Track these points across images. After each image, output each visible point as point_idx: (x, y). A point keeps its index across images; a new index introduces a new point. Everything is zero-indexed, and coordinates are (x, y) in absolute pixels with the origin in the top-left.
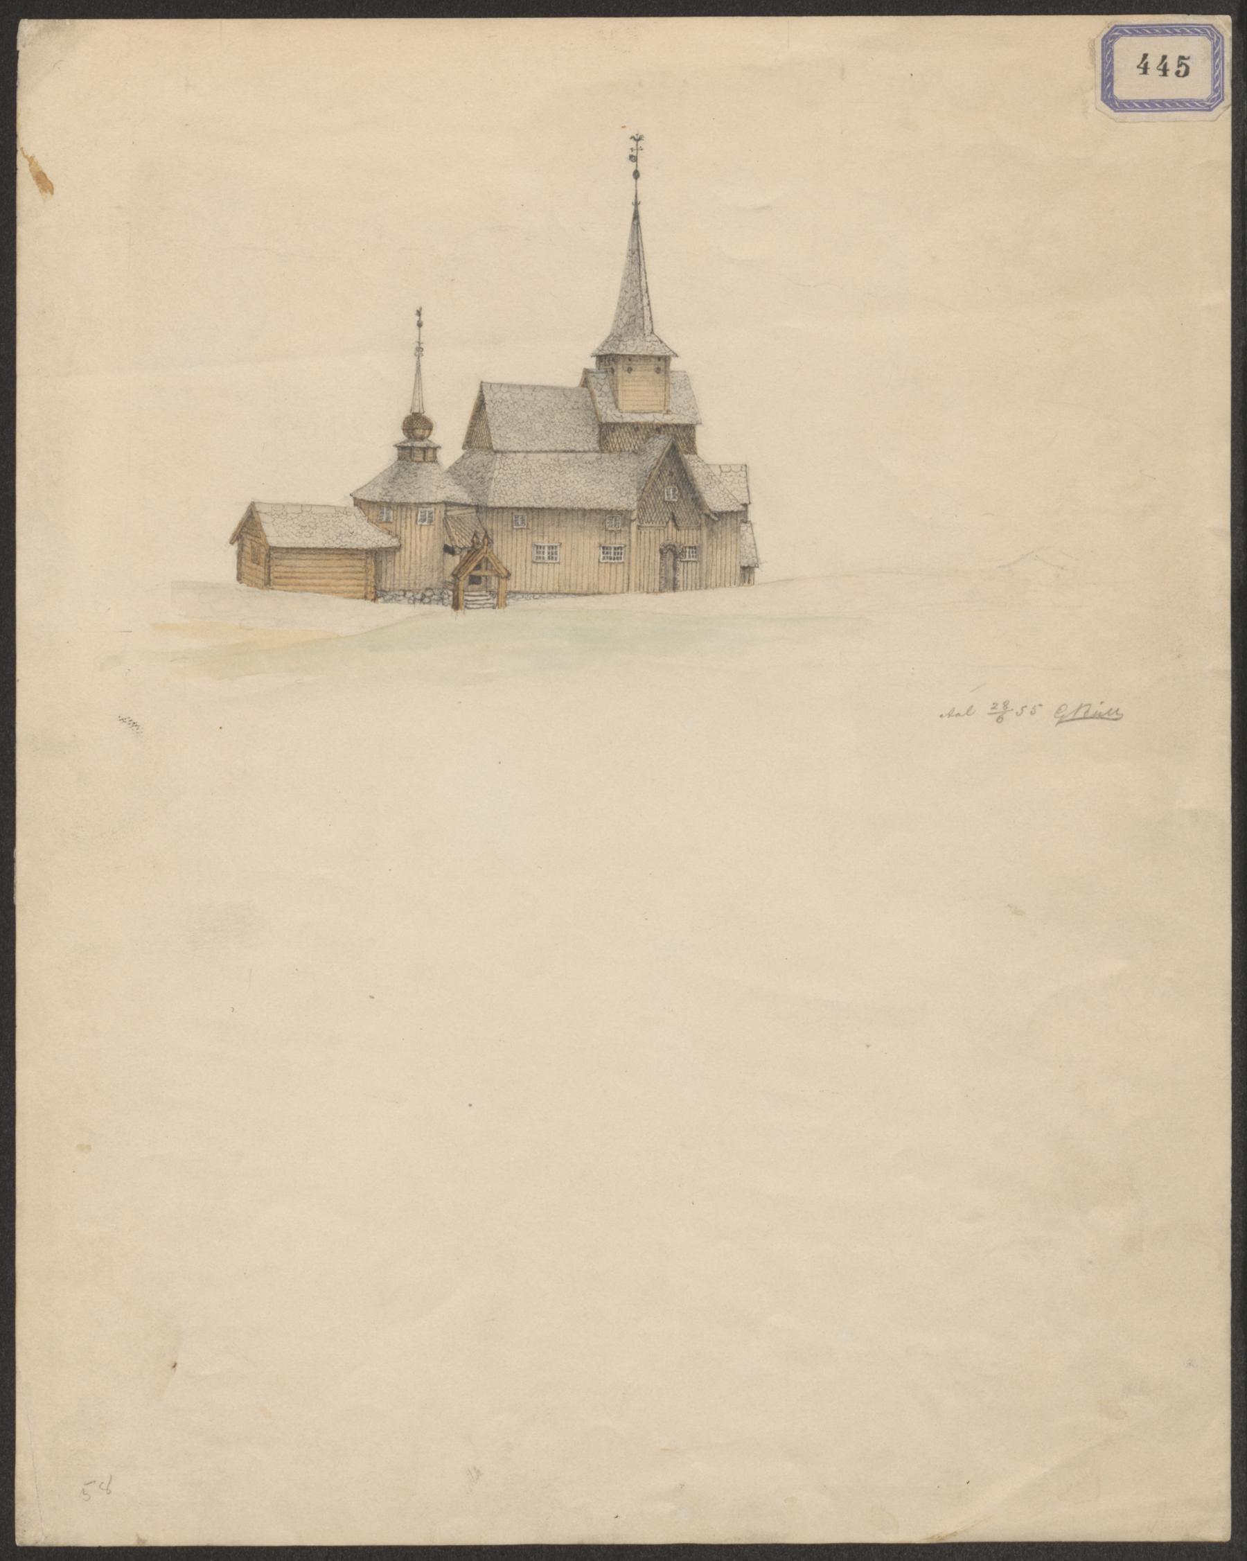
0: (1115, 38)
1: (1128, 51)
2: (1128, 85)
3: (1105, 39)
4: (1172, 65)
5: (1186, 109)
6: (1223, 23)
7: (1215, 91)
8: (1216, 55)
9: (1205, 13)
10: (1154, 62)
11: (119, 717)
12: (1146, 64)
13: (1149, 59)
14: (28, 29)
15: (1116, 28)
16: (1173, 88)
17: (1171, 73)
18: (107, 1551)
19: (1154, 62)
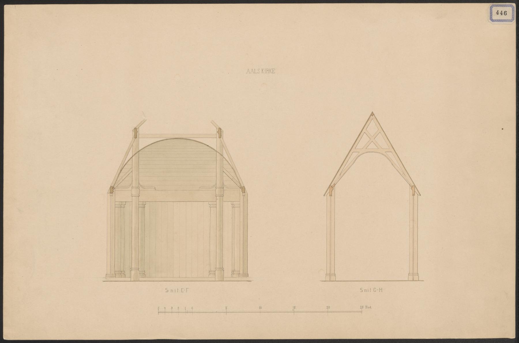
0: (492, 7)
1: (495, 10)
2: (495, 17)
3: (490, 7)
4: (503, 13)
5: (502, 21)
6: (514, 5)
7: (513, 18)
8: (513, 11)
9: (497, 3)
10: (500, 12)
11: (295, 307)
12: (502, 13)
13: (498, 11)
14: (9, 10)
15: (493, 5)
16: (503, 17)
17: (503, 14)
18: (2, 278)
19: (500, 12)
